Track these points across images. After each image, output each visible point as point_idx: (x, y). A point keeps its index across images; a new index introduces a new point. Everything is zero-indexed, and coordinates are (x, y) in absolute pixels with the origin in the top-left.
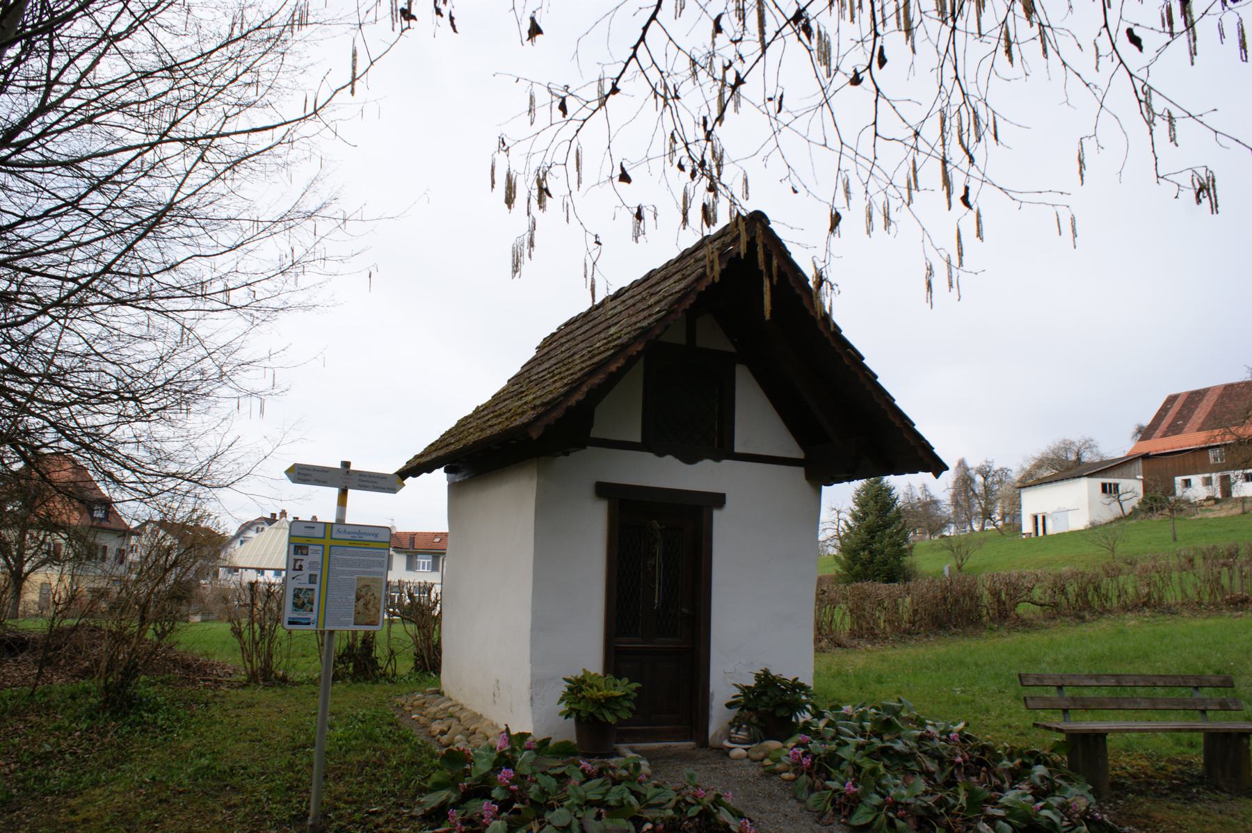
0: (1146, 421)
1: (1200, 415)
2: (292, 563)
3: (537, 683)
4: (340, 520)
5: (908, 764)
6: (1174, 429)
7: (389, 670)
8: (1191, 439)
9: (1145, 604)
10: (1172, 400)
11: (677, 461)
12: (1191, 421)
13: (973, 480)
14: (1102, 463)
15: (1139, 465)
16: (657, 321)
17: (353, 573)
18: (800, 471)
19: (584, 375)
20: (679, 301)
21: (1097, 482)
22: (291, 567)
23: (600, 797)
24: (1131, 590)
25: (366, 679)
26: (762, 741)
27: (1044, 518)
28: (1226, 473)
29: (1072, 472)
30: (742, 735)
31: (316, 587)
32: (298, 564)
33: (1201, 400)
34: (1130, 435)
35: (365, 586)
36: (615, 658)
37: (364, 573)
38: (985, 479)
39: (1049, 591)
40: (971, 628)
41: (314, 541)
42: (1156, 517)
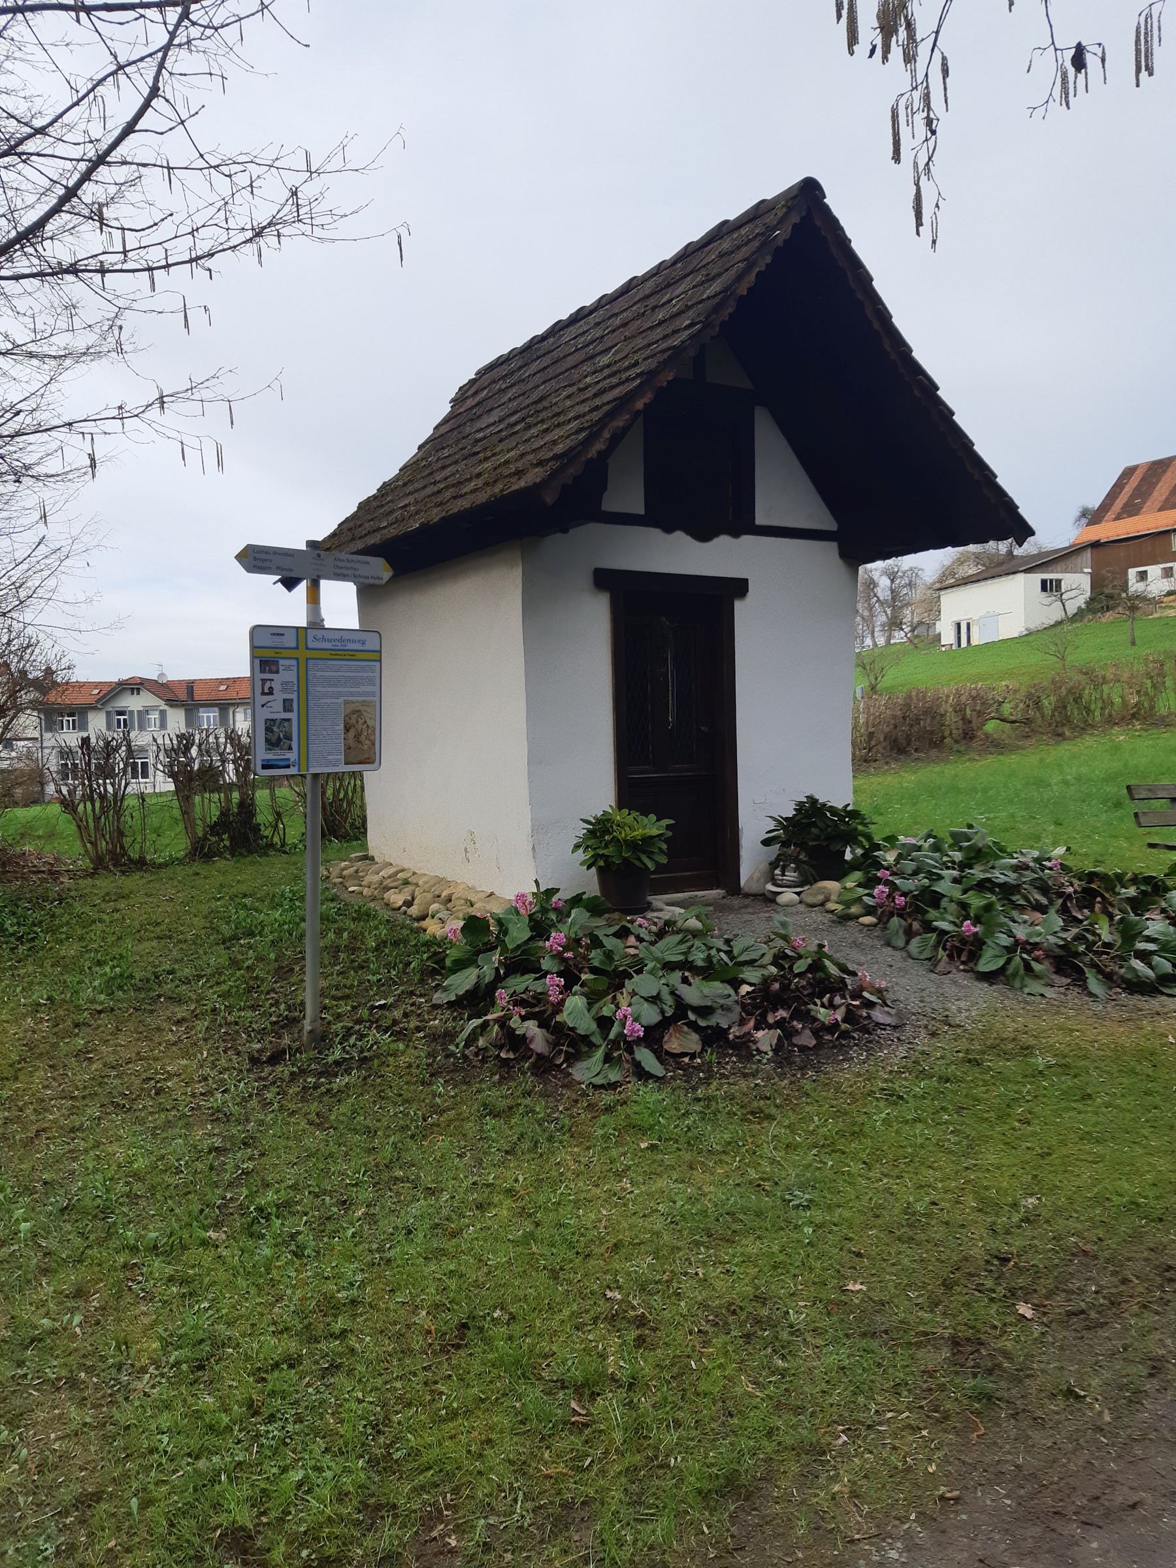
0: (1095, 502)
1: (1161, 491)
2: (258, 684)
3: (539, 829)
4: (316, 622)
5: (1014, 898)
6: (1131, 510)
7: (276, 839)
8: (1148, 521)
9: (1134, 716)
10: (1129, 472)
11: (689, 538)
12: (1152, 498)
13: (875, 585)
14: (1040, 555)
15: (1088, 555)
16: (691, 337)
17: (339, 695)
18: (833, 546)
19: (606, 415)
20: (717, 308)
21: (1037, 578)
22: (258, 690)
23: (681, 958)
24: (1117, 700)
25: (250, 852)
26: (816, 881)
27: (968, 625)
28: (1169, 565)
29: (1004, 567)
30: (791, 876)
31: (293, 716)
32: (268, 685)
33: (1164, 472)
34: (1072, 520)
35: (354, 712)
36: (629, 793)
37: (352, 694)
38: (892, 581)
39: (1021, 706)
40: (934, 752)
41: (285, 653)
42: (1109, 616)
